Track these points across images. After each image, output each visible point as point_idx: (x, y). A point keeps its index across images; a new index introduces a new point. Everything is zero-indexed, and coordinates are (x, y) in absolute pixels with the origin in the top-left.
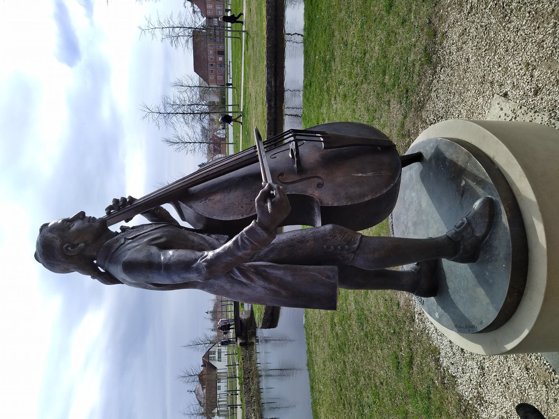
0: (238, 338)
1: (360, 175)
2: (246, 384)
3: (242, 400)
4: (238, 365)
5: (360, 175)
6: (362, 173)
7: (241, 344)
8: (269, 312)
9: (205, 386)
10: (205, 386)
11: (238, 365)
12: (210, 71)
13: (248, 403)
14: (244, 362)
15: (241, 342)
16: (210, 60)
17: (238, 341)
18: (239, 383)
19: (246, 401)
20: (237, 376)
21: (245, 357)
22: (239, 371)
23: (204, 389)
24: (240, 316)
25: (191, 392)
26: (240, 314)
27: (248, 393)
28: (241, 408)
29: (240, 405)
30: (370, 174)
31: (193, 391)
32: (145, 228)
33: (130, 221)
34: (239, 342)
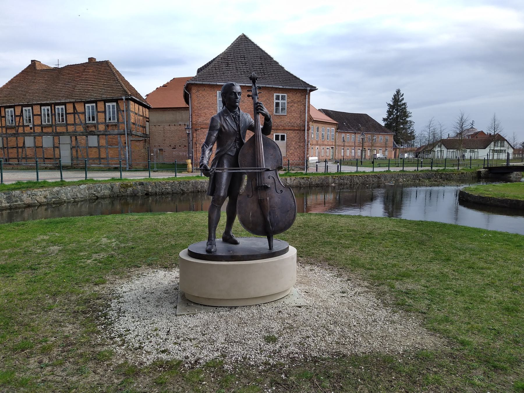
0: (487, 169)
1: (251, 214)
2: (435, 175)
3: (421, 171)
4: (458, 169)
5: (251, 214)
6: (251, 215)
7: (479, 172)
8: (469, 198)
9: (470, 137)
10: (470, 137)
11: (458, 169)
12: (280, 101)
13: (417, 176)
14: (458, 174)
15: (482, 173)
16: (275, 101)
17: (484, 169)
18: (439, 169)
19: (419, 175)
20: (446, 168)
21: (464, 176)
22: (451, 170)
23: (468, 137)
24: (515, 172)
25: (472, 124)
26: (518, 173)
27: (427, 177)
28: (415, 170)
29: (418, 169)
30: (251, 219)
31: (473, 126)
32: (44, 117)
33: (275, 59)
34: (482, 170)
